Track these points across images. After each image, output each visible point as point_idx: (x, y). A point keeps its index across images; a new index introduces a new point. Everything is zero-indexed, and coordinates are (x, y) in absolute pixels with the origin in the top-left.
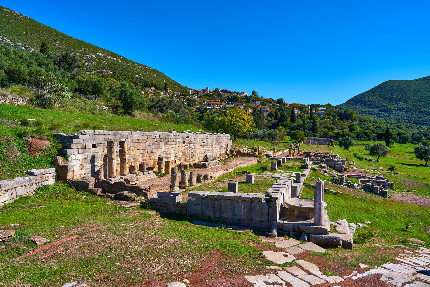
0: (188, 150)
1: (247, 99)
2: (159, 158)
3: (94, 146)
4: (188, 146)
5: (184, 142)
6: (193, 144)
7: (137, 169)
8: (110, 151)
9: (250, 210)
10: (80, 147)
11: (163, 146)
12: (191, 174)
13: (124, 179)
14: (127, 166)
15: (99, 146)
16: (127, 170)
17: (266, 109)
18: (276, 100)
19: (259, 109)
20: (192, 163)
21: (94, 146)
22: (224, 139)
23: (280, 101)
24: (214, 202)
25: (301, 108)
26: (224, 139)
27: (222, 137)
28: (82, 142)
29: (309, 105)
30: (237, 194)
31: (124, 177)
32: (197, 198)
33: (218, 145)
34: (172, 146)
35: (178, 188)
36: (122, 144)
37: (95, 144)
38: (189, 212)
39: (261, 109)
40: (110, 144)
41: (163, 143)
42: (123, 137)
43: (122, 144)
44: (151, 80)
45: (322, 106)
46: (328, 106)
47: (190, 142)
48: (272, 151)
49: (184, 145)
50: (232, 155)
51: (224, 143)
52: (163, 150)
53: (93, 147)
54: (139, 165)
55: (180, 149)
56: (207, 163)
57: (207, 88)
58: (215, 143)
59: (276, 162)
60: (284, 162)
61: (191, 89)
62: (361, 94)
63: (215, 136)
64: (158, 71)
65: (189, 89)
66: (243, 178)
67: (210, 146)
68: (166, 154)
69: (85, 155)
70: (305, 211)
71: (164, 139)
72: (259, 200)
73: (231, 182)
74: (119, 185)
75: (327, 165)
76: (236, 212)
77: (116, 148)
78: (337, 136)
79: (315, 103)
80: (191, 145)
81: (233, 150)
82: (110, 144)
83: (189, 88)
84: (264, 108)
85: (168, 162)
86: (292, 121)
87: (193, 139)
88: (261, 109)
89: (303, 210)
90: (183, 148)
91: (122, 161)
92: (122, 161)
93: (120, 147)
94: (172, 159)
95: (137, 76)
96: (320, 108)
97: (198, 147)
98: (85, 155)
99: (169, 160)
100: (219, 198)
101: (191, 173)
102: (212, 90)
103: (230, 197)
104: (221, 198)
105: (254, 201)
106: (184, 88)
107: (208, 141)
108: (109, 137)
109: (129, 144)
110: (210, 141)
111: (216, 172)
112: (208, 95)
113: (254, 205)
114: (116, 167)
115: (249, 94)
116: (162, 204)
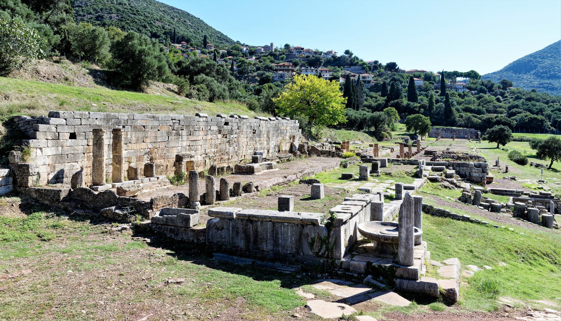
0: (227, 144)
1: (335, 62)
2: (177, 156)
3: (73, 136)
4: (226, 137)
5: (220, 132)
6: (236, 136)
7: (140, 171)
8: (96, 144)
9: (300, 237)
10: (50, 138)
11: (185, 138)
12: (223, 182)
13: (118, 188)
14: (125, 167)
15: (80, 135)
16: (124, 174)
17: (367, 79)
18: (384, 64)
19: (356, 80)
20: (232, 166)
21: (73, 136)
22: (288, 128)
23: (392, 66)
24: (246, 225)
25: (428, 77)
26: (288, 128)
27: (285, 125)
28: (54, 129)
29: (439, 73)
30: (290, 214)
31: (118, 185)
32: (221, 218)
33: (277, 137)
34: (200, 138)
35: (198, 203)
36: (116, 134)
37: (75, 133)
38: (209, 239)
39: (359, 78)
40: (97, 132)
41: (184, 133)
42: (120, 122)
43: (116, 134)
44: (182, 31)
45: (461, 75)
46: (472, 75)
47: (231, 132)
48: (372, 148)
49: (220, 136)
50: (302, 153)
51: (288, 134)
52: (185, 144)
53: (70, 138)
54: (143, 167)
55: (213, 141)
56: (256, 166)
57: (272, 45)
58: (273, 134)
59: (369, 166)
60: (383, 166)
61: (247, 46)
62: (531, 56)
63: (272, 122)
64: (192, 16)
65: (243, 45)
66: (308, 190)
67: (264, 138)
68: (190, 150)
69: (57, 150)
70: (386, 242)
71: (188, 126)
72: (314, 223)
73: (283, 196)
74: (106, 196)
75: (458, 173)
76: (280, 241)
77: (107, 139)
78: (489, 123)
79: (450, 70)
80: (232, 136)
81: (304, 146)
82: (97, 132)
83: (242, 43)
84: (364, 77)
85: (192, 162)
86: (412, 97)
87: (235, 127)
88: (359, 78)
89: (382, 240)
90: (218, 142)
91: (117, 160)
92: (117, 160)
93: (114, 138)
94: (198, 158)
95: (158, 24)
96: (458, 79)
97: (243, 140)
98: (57, 150)
99: (192, 159)
100: (254, 219)
101: (380, 200)
102: (279, 47)
103: (270, 217)
104: (256, 219)
105: (307, 225)
106: (235, 43)
107: (261, 131)
108: (98, 122)
109: (129, 133)
110: (264, 130)
111: (264, 179)
112: (271, 54)
113: (306, 230)
114: (107, 169)
115: (340, 53)
116: (169, 227)
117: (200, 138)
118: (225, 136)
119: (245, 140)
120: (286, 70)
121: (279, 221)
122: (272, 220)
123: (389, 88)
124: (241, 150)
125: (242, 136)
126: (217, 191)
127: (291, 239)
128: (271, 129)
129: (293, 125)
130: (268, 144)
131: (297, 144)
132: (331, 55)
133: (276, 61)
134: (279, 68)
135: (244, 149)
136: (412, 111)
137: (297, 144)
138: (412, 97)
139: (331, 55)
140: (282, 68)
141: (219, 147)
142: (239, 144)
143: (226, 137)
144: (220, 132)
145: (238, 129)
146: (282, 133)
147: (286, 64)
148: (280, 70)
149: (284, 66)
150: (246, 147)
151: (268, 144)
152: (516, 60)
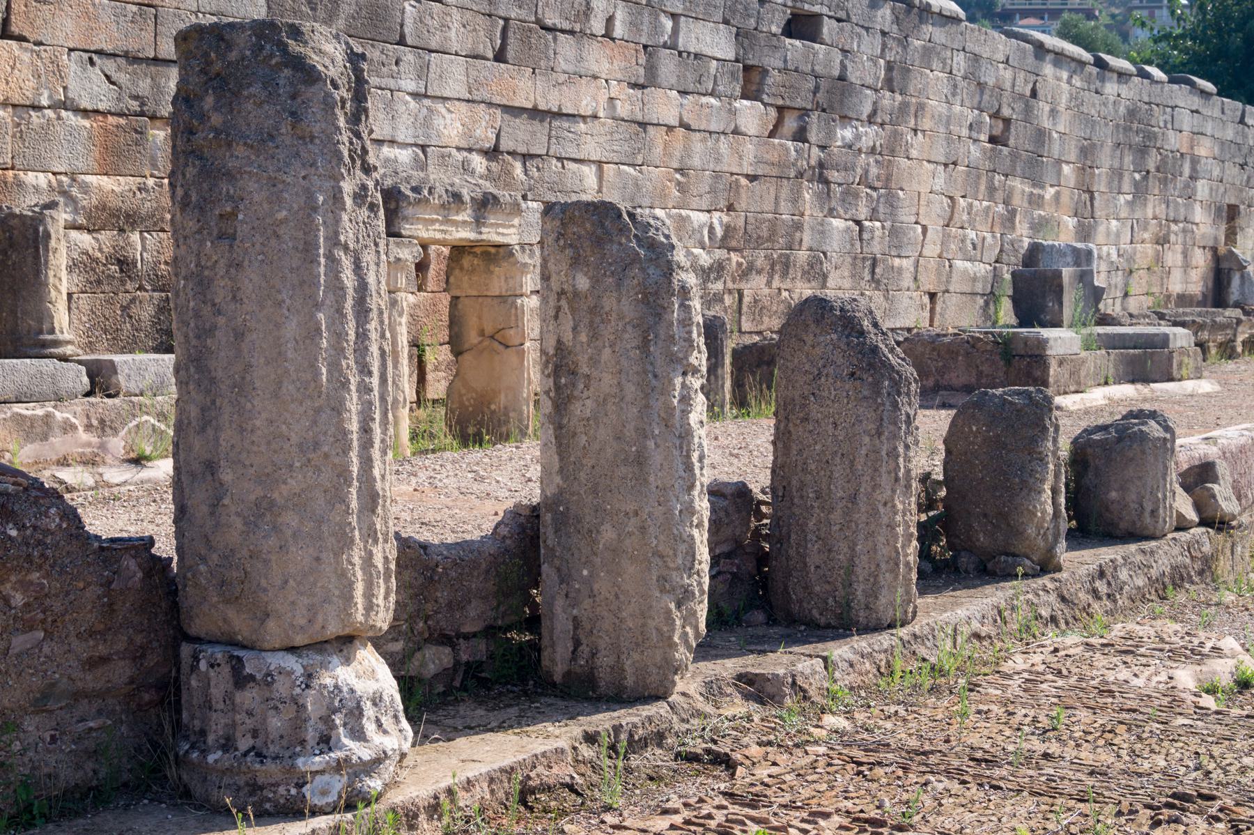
6: (870, 135)
35: (369, 675)
47: (835, 97)
49: (751, 115)
58: (1117, 173)
63: (1111, 88)
97: (925, 183)
107: (1041, 136)
117: (586, 99)
118: (791, 120)
124: (912, 252)
125: (917, 145)
126: (732, 500)
128: (1106, 137)
129: (1230, 133)
135: (932, 250)
141: (742, 204)
142: (891, 202)
143: (800, 136)
144: (752, 81)
145: (889, 84)
151: (1085, 232)
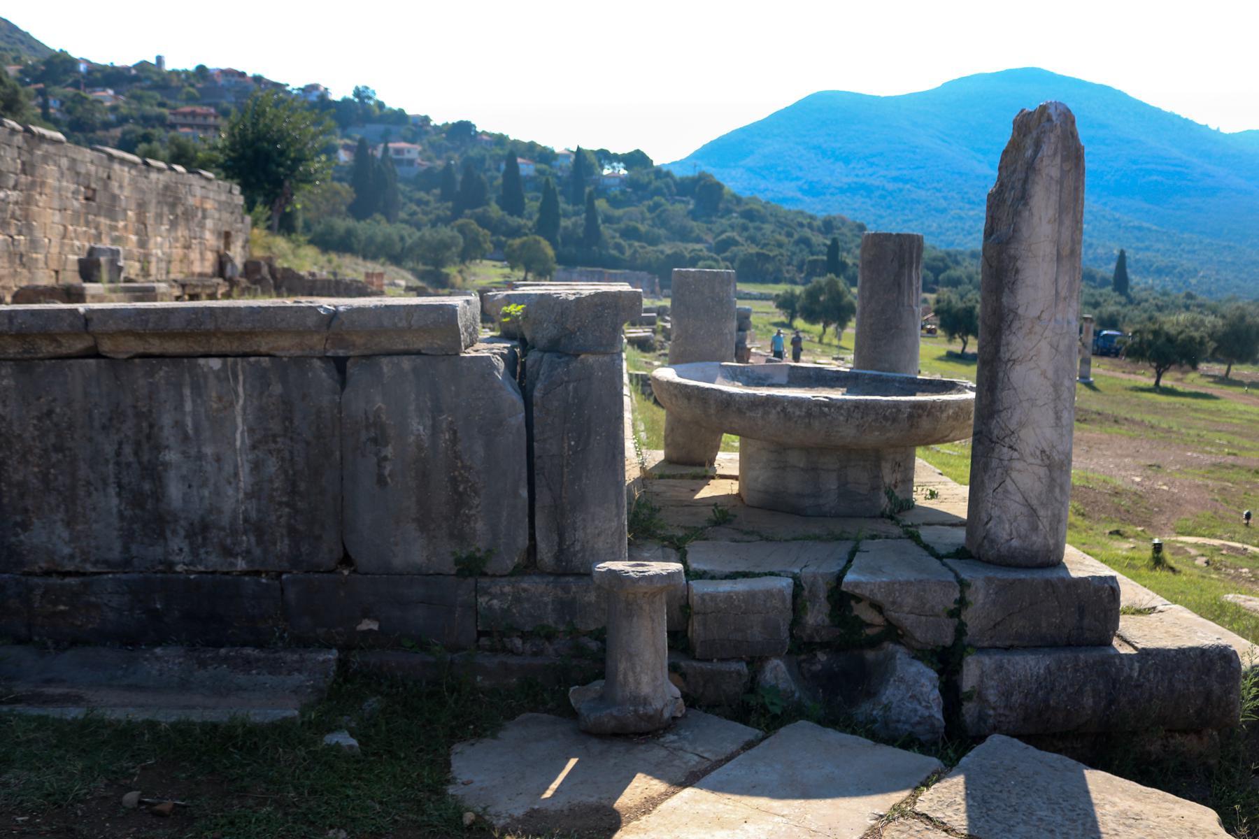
17: (407, 156)
46: (636, 160)
58: (159, 216)
62: (742, 130)
84: (398, 151)
107: (114, 198)
113: (369, 398)
119: (57, 217)
120: (199, 127)
121: (156, 346)
122: (106, 346)
123: (459, 177)
125: (42, 200)
127: (256, 466)
130: (142, 244)
131: (237, 254)
132: (316, 93)
133: (171, 102)
134: (180, 119)
136: (515, 232)
137: (237, 254)
138: (512, 203)
139: (316, 93)
140: (190, 120)
146: (188, 215)
147: (204, 110)
148: (183, 125)
149: (193, 114)
150: (62, 245)
152: (714, 138)
